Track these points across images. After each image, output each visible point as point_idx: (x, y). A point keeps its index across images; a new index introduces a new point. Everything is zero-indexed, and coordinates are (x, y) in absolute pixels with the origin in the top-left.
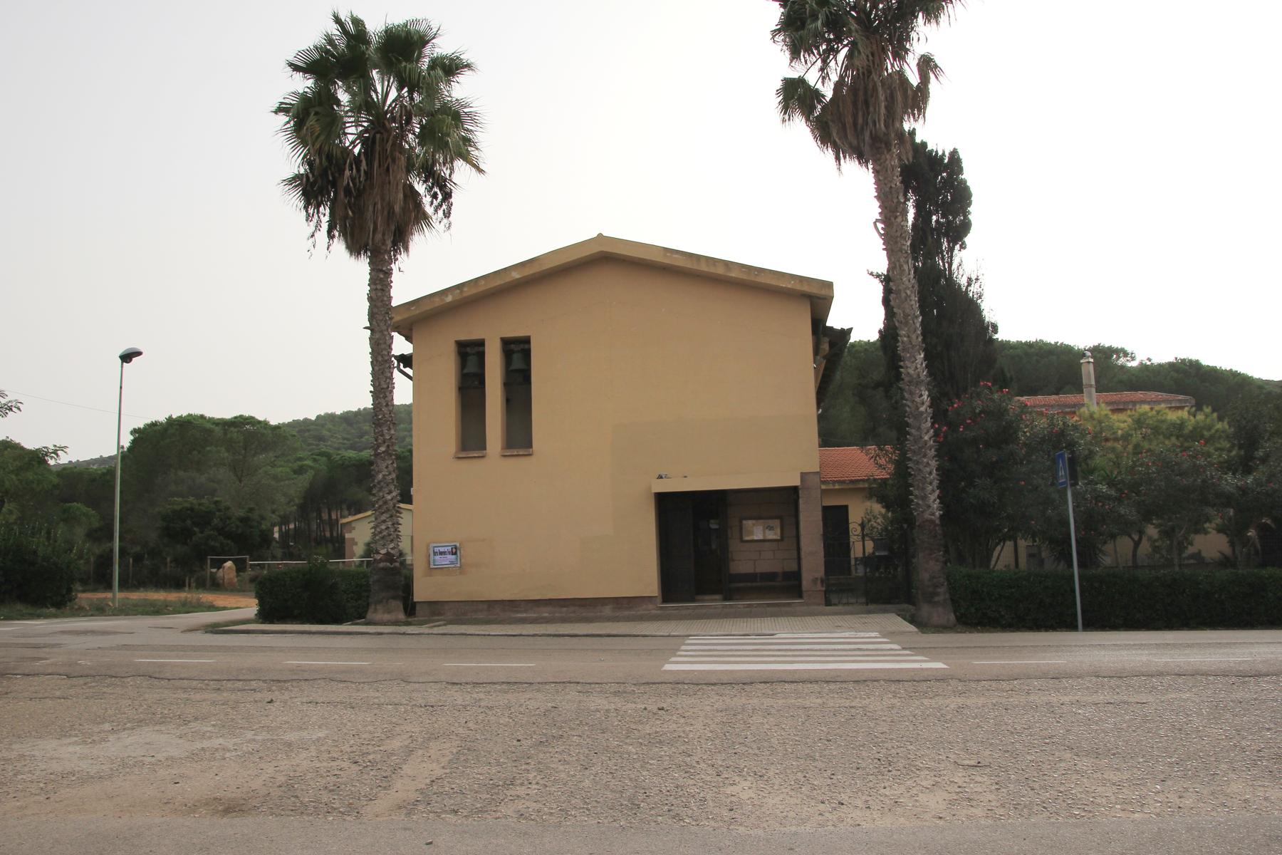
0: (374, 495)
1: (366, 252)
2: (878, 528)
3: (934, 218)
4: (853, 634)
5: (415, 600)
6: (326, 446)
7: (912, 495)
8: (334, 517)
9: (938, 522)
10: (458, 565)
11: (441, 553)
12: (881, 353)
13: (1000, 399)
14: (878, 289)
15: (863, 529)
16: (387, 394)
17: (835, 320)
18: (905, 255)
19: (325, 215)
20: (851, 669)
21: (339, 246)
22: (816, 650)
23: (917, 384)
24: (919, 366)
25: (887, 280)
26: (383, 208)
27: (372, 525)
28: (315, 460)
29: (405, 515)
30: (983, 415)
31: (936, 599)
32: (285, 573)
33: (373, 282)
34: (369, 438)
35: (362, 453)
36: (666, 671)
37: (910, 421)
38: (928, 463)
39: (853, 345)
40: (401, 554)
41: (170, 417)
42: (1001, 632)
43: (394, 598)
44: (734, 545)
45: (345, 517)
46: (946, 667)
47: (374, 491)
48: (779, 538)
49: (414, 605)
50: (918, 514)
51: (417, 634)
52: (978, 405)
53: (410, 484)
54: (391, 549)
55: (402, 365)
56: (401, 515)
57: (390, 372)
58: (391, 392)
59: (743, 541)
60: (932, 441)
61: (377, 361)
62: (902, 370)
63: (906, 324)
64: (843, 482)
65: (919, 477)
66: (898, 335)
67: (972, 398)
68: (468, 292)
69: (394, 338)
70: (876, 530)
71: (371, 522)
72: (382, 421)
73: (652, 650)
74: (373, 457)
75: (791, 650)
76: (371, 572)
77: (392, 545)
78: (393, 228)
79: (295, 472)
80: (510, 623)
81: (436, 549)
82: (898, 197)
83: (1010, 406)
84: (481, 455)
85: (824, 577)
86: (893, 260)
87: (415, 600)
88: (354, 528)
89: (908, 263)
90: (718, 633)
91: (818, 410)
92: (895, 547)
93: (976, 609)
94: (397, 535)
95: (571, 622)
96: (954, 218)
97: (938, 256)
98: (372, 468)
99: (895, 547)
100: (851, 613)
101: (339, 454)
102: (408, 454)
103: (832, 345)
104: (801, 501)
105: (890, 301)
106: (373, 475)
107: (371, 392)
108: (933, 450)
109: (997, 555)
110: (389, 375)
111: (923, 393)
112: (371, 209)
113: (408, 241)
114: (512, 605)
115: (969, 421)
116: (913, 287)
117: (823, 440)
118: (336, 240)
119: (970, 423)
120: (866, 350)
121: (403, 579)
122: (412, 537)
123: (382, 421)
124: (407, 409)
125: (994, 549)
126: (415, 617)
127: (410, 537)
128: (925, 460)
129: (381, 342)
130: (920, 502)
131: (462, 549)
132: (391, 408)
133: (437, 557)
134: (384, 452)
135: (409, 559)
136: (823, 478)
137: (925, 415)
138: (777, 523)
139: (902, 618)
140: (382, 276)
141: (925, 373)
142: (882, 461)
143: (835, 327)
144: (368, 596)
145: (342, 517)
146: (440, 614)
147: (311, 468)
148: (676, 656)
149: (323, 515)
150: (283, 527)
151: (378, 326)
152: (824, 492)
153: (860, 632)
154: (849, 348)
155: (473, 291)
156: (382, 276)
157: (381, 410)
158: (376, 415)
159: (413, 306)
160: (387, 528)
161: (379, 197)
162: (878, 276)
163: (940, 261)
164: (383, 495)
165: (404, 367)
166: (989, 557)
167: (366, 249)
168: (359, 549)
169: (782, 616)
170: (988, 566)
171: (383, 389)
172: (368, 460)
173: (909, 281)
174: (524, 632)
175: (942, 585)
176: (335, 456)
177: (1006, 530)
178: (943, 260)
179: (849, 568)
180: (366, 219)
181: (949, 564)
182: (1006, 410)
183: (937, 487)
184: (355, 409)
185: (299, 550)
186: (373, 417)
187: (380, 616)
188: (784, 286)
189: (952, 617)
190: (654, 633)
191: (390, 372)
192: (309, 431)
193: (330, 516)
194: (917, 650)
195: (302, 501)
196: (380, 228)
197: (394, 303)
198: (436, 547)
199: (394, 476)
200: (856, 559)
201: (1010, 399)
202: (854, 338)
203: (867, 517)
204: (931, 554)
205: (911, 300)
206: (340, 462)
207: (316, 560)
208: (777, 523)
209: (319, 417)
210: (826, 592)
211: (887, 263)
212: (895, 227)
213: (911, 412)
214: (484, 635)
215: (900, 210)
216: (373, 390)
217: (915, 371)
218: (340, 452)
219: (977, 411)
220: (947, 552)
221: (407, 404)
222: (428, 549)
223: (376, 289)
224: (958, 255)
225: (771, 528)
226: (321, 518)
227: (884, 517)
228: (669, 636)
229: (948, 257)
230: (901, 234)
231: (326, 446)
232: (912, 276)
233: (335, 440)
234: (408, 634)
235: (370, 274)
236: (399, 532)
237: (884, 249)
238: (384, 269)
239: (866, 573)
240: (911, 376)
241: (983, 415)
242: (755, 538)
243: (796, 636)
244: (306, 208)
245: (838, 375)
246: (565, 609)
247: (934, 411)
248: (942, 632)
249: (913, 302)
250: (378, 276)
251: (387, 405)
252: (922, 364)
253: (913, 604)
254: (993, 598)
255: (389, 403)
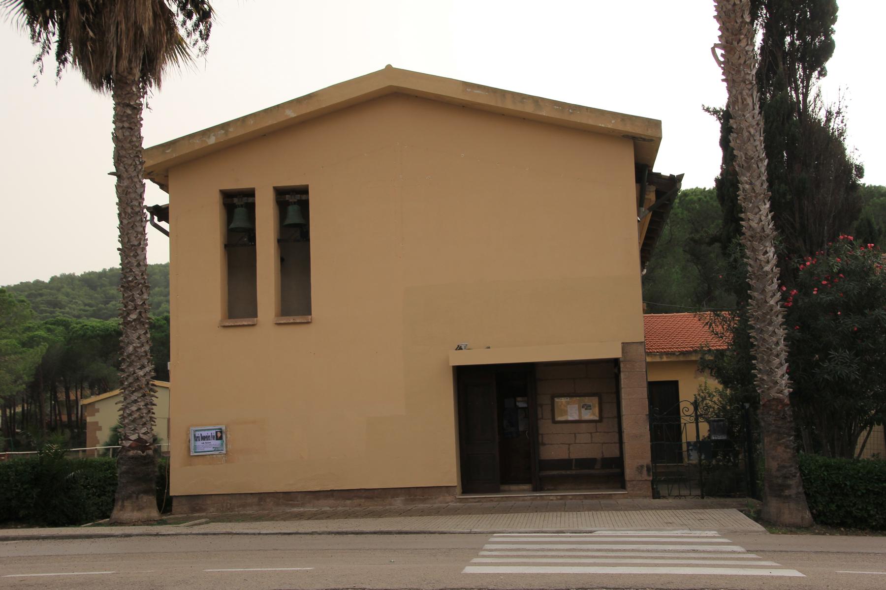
0: (123, 370)
1: (108, 82)
2: (714, 408)
3: (788, 39)
4: (686, 532)
5: (171, 494)
6: (63, 313)
7: (755, 369)
8: (72, 397)
9: (787, 401)
10: (224, 452)
11: (204, 438)
12: (716, 203)
13: (864, 256)
14: (715, 127)
15: (696, 409)
16: (139, 252)
17: (663, 166)
18: (750, 87)
19: (54, 34)
20: (684, 575)
21: (74, 74)
22: (643, 551)
23: (761, 240)
24: (763, 218)
25: (726, 117)
26: (128, 29)
27: (120, 406)
28: (49, 330)
29: (160, 393)
30: (841, 275)
31: (787, 493)
32: (9, 467)
33: (118, 118)
34: (117, 304)
35: (108, 322)
36: (467, 574)
37: (752, 282)
38: (774, 332)
39: (686, 194)
40: (155, 440)
41: (74, 274)
42: (870, 535)
43: (146, 492)
44: (545, 427)
45: (86, 397)
46: (800, 575)
47: (123, 366)
48: (597, 418)
49: (170, 499)
50: (762, 391)
51: (173, 535)
52: (836, 263)
53: (167, 357)
54: (144, 434)
55: (156, 218)
56: (156, 394)
57: (142, 226)
58: (144, 249)
59: (555, 422)
60: (779, 306)
61: (125, 213)
62: (742, 223)
63: (749, 168)
64: (673, 354)
65: (763, 349)
66: (738, 182)
67: (828, 255)
68: (234, 133)
69: (146, 186)
70: (711, 410)
71: (120, 402)
72: (133, 284)
73: (450, 550)
74: (121, 326)
75: (613, 551)
76: (118, 463)
77: (144, 430)
78: (142, 54)
79: (24, 344)
80: (284, 520)
81: (198, 434)
82: (742, 16)
83: (876, 264)
84: (250, 323)
85: (650, 463)
86: (734, 92)
87: (171, 494)
88: (98, 411)
89: (752, 95)
90: (527, 529)
91: (642, 271)
92: (736, 430)
93: (837, 506)
94: (151, 418)
95: (356, 517)
96: (813, 39)
97: (790, 85)
98: (121, 338)
99: (736, 430)
100: (684, 508)
101: (80, 323)
102: (165, 322)
103: (658, 194)
104: (622, 375)
105: (730, 142)
106: (122, 348)
107: (119, 249)
108: (780, 316)
109: (862, 441)
110: (141, 229)
111: (768, 249)
112: (113, 29)
113: (160, 72)
114: (288, 497)
115: (824, 282)
116: (758, 124)
117: (648, 305)
118: (69, 65)
119: (826, 285)
120: (700, 199)
121: (157, 469)
122: (169, 420)
123: (133, 284)
124: (163, 270)
125: (859, 434)
126: (171, 514)
127: (166, 420)
128: (771, 329)
129: (130, 190)
130: (765, 378)
131: (228, 433)
132: (143, 268)
133: (199, 443)
134: (134, 320)
135: (164, 446)
136: (649, 349)
137: (770, 276)
138: (594, 401)
139: (745, 514)
140: (129, 112)
141: (770, 226)
142: (719, 329)
143: (663, 173)
144: (114, 492)
145: (83, 397)
146: (201, 510)
147: (45, 339)
148: (478, 556)
149: (59, 395)
150: (8, 411)
151: (127, 171)
152: (648, 364)
153: (696, 530)
154: (681, 197)
155: (241, 132)
156: (129, 112)
157: (131, 271)
158: (125, 277)
159: (169, 148)
160: (139, 409)
161: (122, 14)
162: (715, 112)
163: (793, 92)
164: (134, 371)
165: (159, 220)
166: (852, 443)
167: (110, 79)
168: (104, 435)
169: (602, 509)
170: (852, 455)
171: (133, 246)
172: (115, 330)
173: (753, 117)
174: (301, 530)
175: (795, 476)
176: (75, 325)
177: (873, 412)
178: (796, 90)
179: (681, 454)
180: (107, 42)
181: (801, 451)
182: (871, 269)
183: (785, 359)
184: (99, 269)
185: (28, 437)
186: (122, 279)
187: (127, 515)
188: (603, 126)
189: (808, 515)
190: (453, 530)
191: (142, 226)
192: (41, 295)
193: (68, 396)
194: (763, 553)
195: (32, 379)
196: (125, 54)
197: (146, 145)
198: (196, 431)
199: (147, 348)
200: (688, 443)
201: (876, 256)
202: (686, 185)
203: (702, 394)
204: (779, 440)
205: (755, 140)
206: (81, 332)
207: (50, 449)
208: (594, 401)
209: (53, 279)
210: (653, 482)
211: (727, 96)
212: (737, 52)
213: (753, 272)
214: (254, 534)
215: (744, 31)
216: (121, 247)
217: (758, 223)
218: (80, 320)
219: (835, 270)
220: (798, 436)
221: (163, 263)
222: (188, 434)
223: (123, 127)
224: (817, 84)
225: (588, 407)
226: (56, 398)
227: (721, 395)
228: (470, 533)
229: (803, 87)
230: (745, 62)
231: (63, 313)
232: (757, 111)
233: (74, 306)
234: (161, 535)
235: (115, 109)
236: (153, 413)
237: (723, 80)
238: (132, 103)
239: (700, 460)
240: (753, 230)
241: (841, 275)
242: (570, 418)
243: (619, 533)
244: (30, 23)
245: (666, 230)
246: (348, 502)
247: (781, 270)
248: (795, 533)
249: (758, 143)
250: (125, 112)
251: (139, 265)
252: (767, 215)
253: (759, 498)
254: (859, 493)
255: (141, 263)
